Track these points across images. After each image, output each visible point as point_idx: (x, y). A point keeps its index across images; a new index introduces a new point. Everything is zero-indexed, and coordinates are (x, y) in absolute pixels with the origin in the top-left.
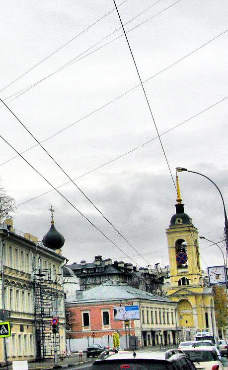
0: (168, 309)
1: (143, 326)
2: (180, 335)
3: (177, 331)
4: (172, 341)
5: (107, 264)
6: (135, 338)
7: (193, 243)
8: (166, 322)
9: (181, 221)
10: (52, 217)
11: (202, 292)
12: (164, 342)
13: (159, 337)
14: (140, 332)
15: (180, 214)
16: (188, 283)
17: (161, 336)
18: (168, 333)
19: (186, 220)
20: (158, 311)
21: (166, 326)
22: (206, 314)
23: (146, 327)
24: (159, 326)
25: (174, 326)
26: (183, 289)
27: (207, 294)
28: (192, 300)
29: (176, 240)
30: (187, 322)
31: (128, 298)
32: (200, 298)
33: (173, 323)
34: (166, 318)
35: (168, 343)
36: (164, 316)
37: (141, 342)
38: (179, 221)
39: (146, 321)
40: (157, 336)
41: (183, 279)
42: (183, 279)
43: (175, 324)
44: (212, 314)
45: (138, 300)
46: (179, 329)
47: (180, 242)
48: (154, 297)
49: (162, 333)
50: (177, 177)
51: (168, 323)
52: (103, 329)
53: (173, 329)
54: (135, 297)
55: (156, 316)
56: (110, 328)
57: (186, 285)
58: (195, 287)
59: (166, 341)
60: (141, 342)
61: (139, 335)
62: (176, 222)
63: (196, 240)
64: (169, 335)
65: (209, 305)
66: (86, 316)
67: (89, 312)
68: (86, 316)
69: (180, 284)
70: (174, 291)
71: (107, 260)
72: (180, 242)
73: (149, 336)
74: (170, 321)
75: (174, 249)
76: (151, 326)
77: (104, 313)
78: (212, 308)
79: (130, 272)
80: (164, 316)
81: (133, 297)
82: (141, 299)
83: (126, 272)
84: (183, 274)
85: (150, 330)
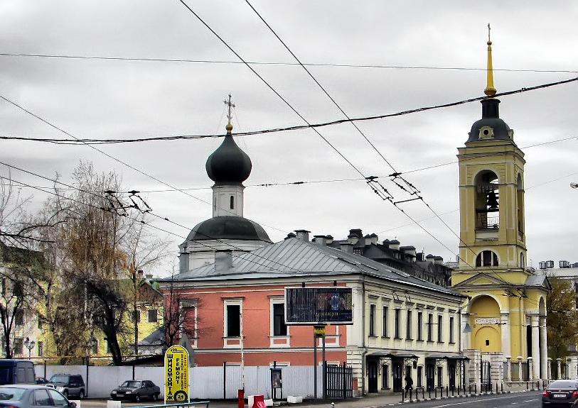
0: (441, 309)
1: (370, 343)
2: (467, 368)
3: (461, 359)
4: (446, 382)
5: (368, 242)
6: (346, 371)
7: (513, 180)
8: (435, 337)
9: (491, 132)
10: (229, 118)
11: (523, 283)
12: (424, 383)
13: (414, 373)
14: (360, 357)
15: (492, 120)
16: (496, 263)
17: (420, 368)
18: (437, 363)
19: (503, 132)
20: (435, 314)
21: (434, 347)
22: (529, 329)
23: (377, 345)
24: (414, 345)
25: (455, 349)
26: (486, 275)
27: (534, 287)
28: (502, 300)
29: (477, 173)
30: (487, 343)
31: (338, 270)
32: (519, 294)
33: (451, 343)
34: (435, 328)
35: (436, 383)
36: (430, 324)
37: (359, 380)
38: (486, 132)
39: (379, 331)
40: (409, 368)
41: (487, 254)
42: (487, 254)
43: (456, 346)
44: (540, 333)
45: (357, 278)
46: (465, 355)
47: (486, 176)
48: (411, 279)
49: (421, 361)
50: (489, 44)
51: (440, 341)
52: (272, 345)
53: (450, 356)
54: (354, 270)
55: (385, 317)
56: (241, 346)
57: (492, 267)
58: (510, 270)
59: (430, 382)
60: (359, 380)
61: (355, 362)
62: (481, 135)
63: (519, 174)
64: (440, 369)
65: (535, 310)
66: (234, 312)
67: (240, 303)
68: (234, 312)
69: (478, 264)
70: (465, 278)
71: (368, 237)
72: (486, 176)
73: (385, 367)
74: (446, 338)
75: (472, 190)
76: (391, 344)
77: (229, 307)
78: (541, 317)
79: (409, 261)
80: (430, 324)
81: (347, 269)
82: (365, 275)
83: (402, 258)
84: (486, 243)
85: (388, 352)
